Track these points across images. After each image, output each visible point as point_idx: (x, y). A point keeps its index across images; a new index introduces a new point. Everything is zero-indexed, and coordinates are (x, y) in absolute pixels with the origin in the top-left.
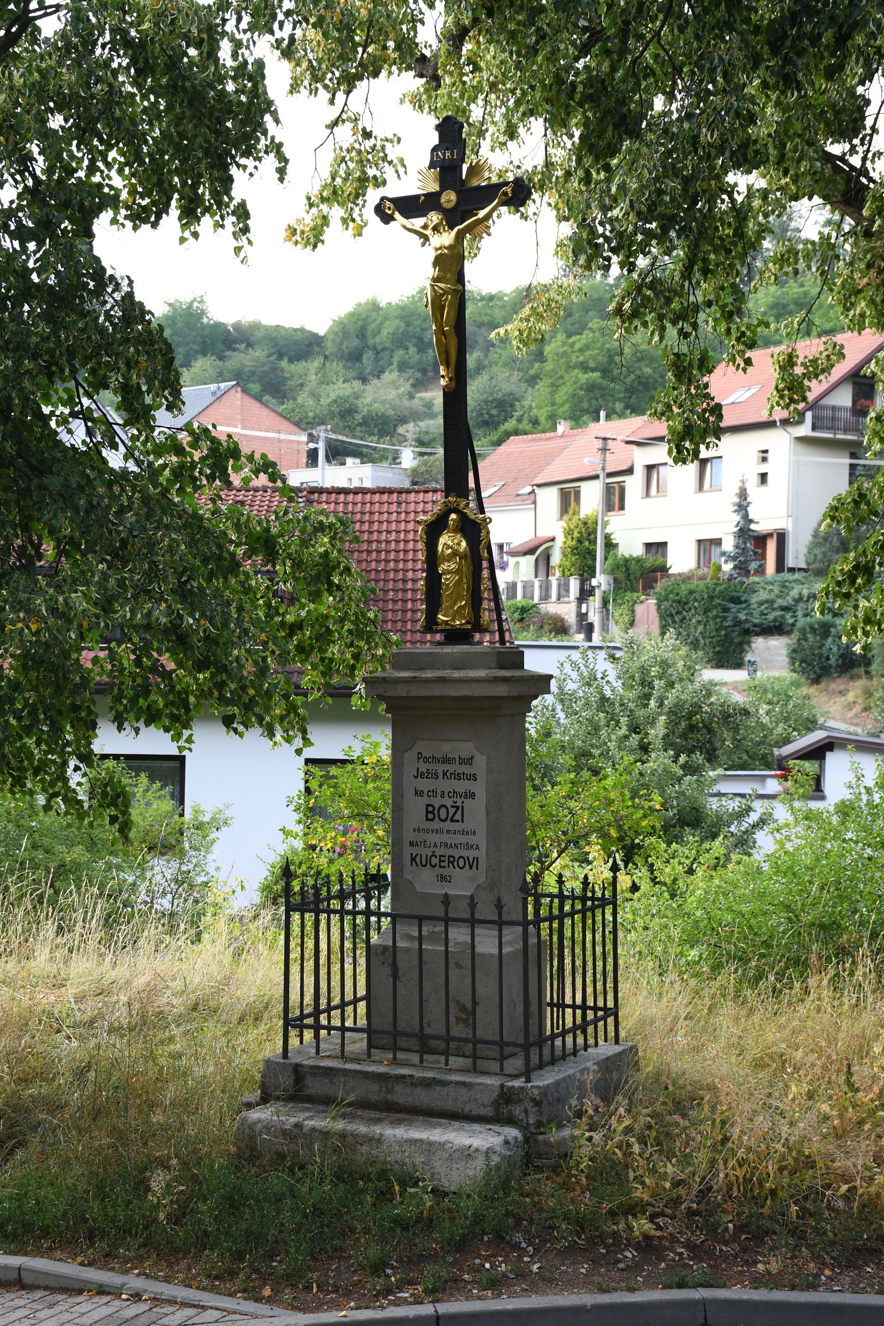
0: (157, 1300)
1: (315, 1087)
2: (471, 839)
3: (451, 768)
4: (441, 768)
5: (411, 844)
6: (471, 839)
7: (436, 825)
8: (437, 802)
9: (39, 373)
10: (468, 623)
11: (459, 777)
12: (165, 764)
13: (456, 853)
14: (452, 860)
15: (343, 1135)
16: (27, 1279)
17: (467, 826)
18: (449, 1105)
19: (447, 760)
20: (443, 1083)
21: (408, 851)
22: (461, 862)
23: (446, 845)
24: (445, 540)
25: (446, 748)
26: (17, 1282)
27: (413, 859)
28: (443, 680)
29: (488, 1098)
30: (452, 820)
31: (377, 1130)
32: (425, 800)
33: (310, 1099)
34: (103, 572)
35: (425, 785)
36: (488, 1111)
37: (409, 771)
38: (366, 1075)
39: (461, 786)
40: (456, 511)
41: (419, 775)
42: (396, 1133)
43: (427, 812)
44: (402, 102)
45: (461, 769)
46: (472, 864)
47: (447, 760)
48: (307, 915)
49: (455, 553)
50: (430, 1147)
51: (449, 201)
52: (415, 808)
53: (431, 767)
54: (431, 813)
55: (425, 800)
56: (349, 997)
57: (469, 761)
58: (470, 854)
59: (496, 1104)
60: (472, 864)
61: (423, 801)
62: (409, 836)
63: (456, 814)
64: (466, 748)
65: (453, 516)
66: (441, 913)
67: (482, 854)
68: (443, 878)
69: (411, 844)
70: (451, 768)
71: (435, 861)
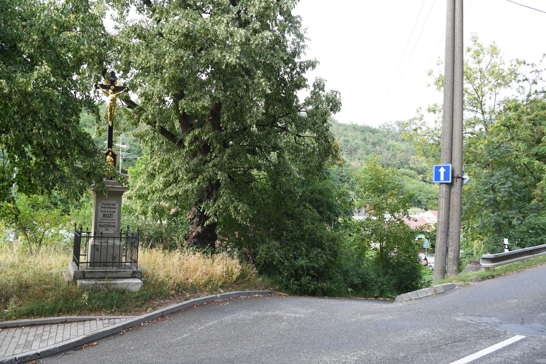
0: (109, 319)
1: (87, 275)
2: (114, 221)
3: (110, 206)
4: (107, 206)
6: (114, 221)
8: (106, 213)
11: (112, 208)
14: (109, 226)
15: (108, 284)
16: (68, 321)
17: (113, 218)
18: (121, 276)
19: (109, 205)
20: (120, 272)
21: (98, 224)
25: (109, 202)
26: (5, 327)
28: (113, 187)
29: (130, 273)
31: (115, 282)
32: (103, 213)
33: (87, 278)
34: (392, 213)
35: (103, 210)
36: (130, 276)
37: (100, 207)
38: (101, 272)
39: (112, 210)
41: (102, 207)
42: (119, 282)
45: (112, 206)
46: (114, 226)
47: (109, 205)
50: (128, 284)
52: (101, 215)
53: (105, 206)
54: (104, 216)
55: (103, 213)
58: (114, 224)
59: (132, 275)
60: (114, 226)
61: (102, 213)
62: (99, 220)
64: (114, 202)
66: (100, 235)
68: (107, 230)
70: (110, 206)
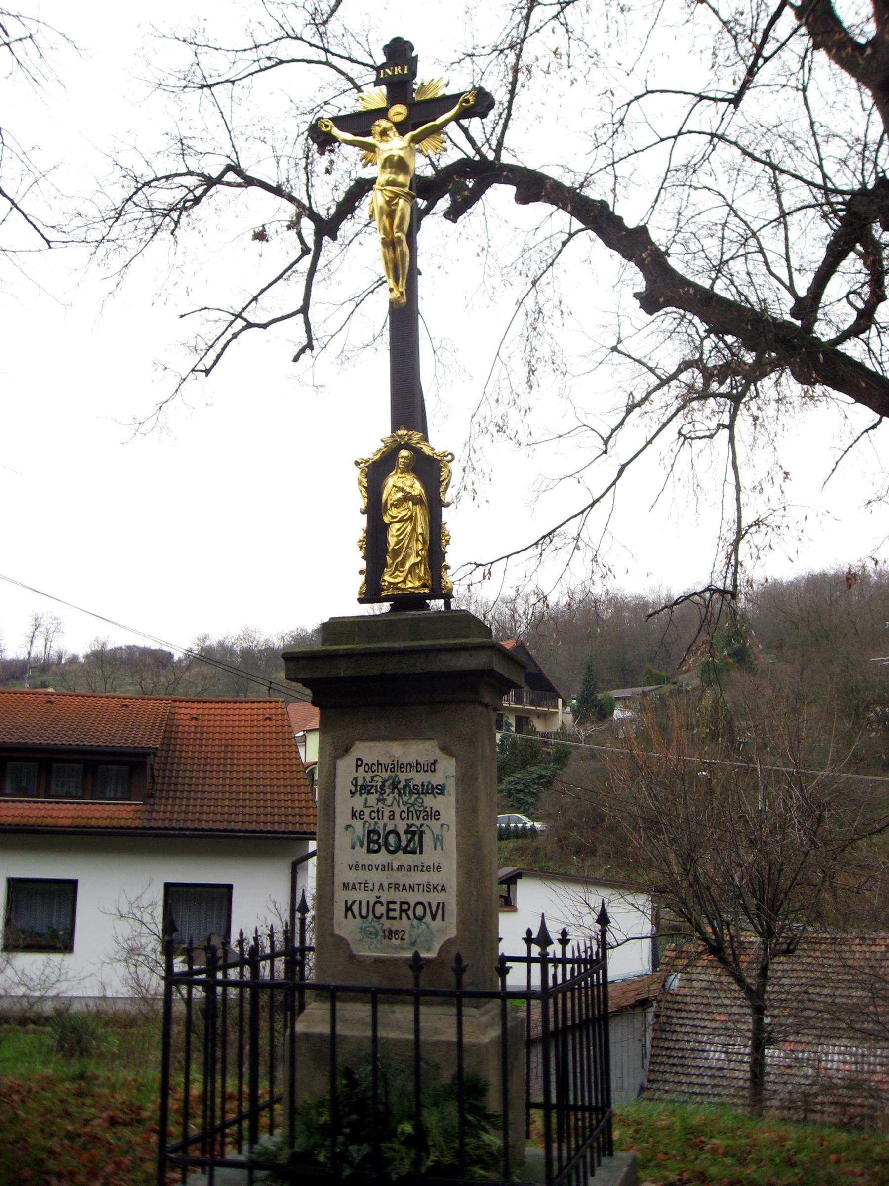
5: (346, 886)
6: (434, 878)
7: (383, 857)
9: (460, 1154)
10: (424, 586)
12: (185, 889)
13: (412, 898)
22: (419, 911)
23: (396, 887)
24: (392, 480)
27: (348, 909)
30: (406, 852)
40: (407, 446)
43: (370, 841)
44: (353, 848)
48: (533, 1002)
49: (407, 497)
51: (399, 114)
56: (265, 1098)
57: (432, 767)
58: (434, 898)
63: (413, 842)
65: (404, 453)
67: (451, 899)
69: (346, 886)
71: (380, 910)
